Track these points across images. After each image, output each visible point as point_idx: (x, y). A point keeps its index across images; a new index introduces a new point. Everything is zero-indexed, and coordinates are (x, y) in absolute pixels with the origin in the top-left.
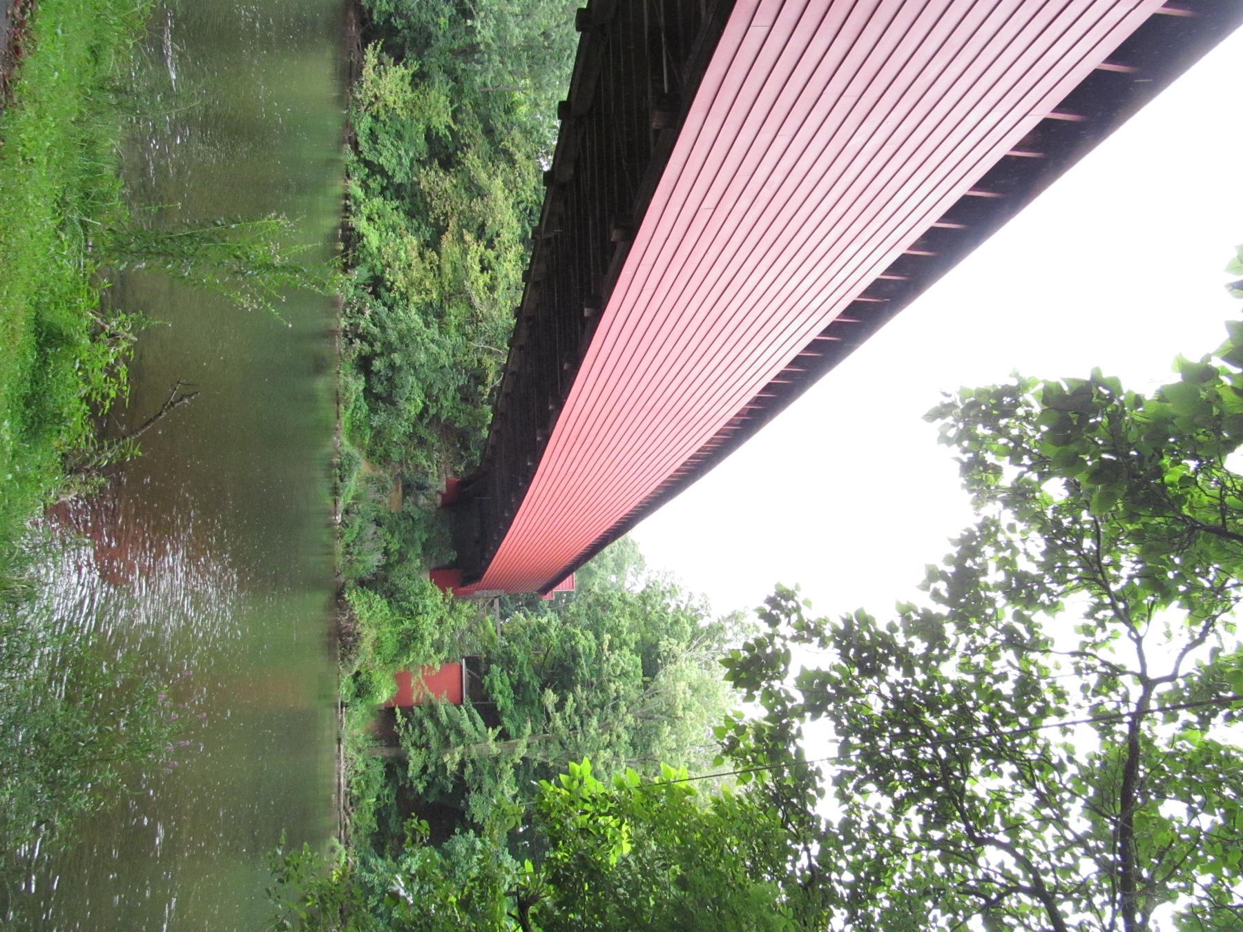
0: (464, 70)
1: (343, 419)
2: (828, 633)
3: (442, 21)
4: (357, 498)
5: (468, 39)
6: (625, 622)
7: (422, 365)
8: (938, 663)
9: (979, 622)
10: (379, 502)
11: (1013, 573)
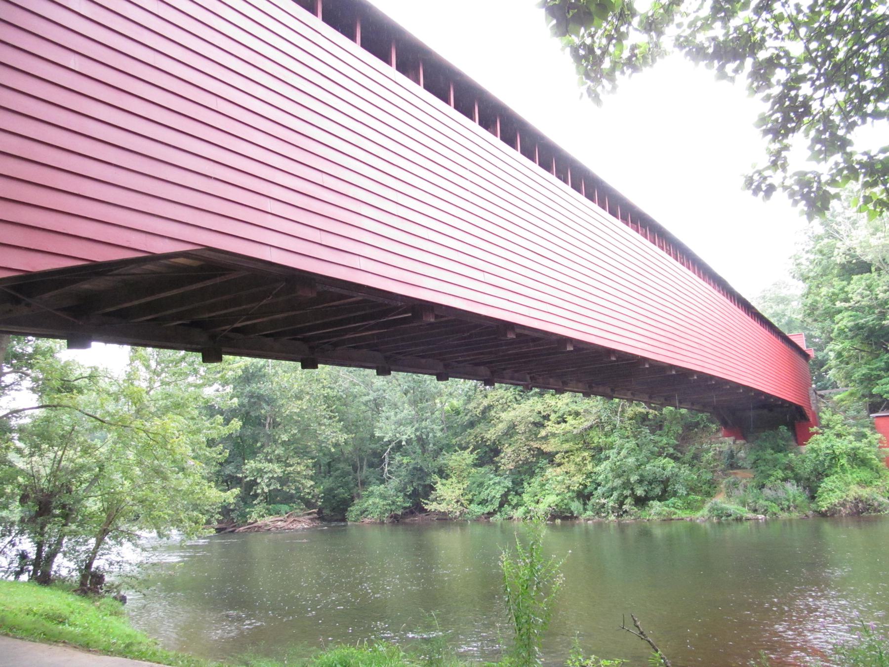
0: (434, 445)
1: (683, 516)
2: (777, 146)
3: (405, 461)
4: (744, 504)
5: (414, 443)
6: (824, 291)
7: (637, 460)
8: (792, 58)
9: (754, 34)
10: (745, 486)
11: (714, 16)
